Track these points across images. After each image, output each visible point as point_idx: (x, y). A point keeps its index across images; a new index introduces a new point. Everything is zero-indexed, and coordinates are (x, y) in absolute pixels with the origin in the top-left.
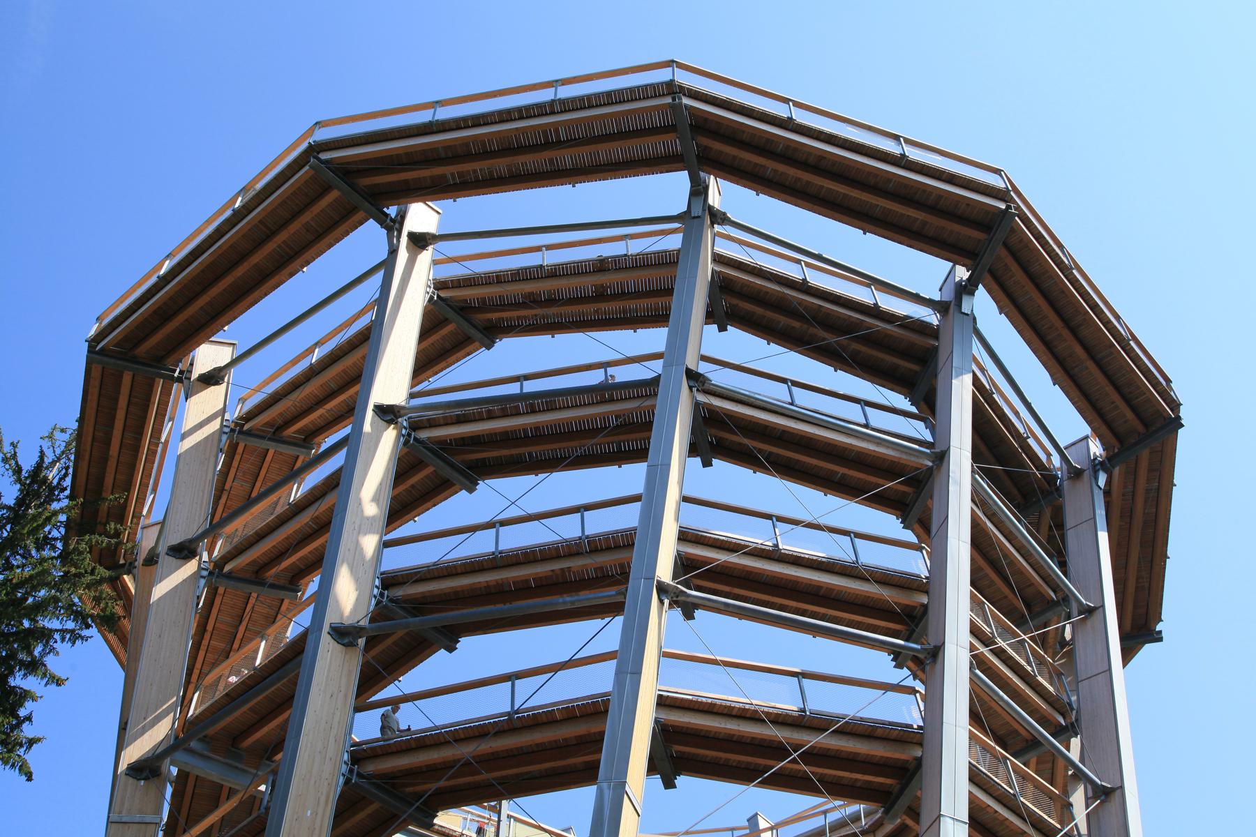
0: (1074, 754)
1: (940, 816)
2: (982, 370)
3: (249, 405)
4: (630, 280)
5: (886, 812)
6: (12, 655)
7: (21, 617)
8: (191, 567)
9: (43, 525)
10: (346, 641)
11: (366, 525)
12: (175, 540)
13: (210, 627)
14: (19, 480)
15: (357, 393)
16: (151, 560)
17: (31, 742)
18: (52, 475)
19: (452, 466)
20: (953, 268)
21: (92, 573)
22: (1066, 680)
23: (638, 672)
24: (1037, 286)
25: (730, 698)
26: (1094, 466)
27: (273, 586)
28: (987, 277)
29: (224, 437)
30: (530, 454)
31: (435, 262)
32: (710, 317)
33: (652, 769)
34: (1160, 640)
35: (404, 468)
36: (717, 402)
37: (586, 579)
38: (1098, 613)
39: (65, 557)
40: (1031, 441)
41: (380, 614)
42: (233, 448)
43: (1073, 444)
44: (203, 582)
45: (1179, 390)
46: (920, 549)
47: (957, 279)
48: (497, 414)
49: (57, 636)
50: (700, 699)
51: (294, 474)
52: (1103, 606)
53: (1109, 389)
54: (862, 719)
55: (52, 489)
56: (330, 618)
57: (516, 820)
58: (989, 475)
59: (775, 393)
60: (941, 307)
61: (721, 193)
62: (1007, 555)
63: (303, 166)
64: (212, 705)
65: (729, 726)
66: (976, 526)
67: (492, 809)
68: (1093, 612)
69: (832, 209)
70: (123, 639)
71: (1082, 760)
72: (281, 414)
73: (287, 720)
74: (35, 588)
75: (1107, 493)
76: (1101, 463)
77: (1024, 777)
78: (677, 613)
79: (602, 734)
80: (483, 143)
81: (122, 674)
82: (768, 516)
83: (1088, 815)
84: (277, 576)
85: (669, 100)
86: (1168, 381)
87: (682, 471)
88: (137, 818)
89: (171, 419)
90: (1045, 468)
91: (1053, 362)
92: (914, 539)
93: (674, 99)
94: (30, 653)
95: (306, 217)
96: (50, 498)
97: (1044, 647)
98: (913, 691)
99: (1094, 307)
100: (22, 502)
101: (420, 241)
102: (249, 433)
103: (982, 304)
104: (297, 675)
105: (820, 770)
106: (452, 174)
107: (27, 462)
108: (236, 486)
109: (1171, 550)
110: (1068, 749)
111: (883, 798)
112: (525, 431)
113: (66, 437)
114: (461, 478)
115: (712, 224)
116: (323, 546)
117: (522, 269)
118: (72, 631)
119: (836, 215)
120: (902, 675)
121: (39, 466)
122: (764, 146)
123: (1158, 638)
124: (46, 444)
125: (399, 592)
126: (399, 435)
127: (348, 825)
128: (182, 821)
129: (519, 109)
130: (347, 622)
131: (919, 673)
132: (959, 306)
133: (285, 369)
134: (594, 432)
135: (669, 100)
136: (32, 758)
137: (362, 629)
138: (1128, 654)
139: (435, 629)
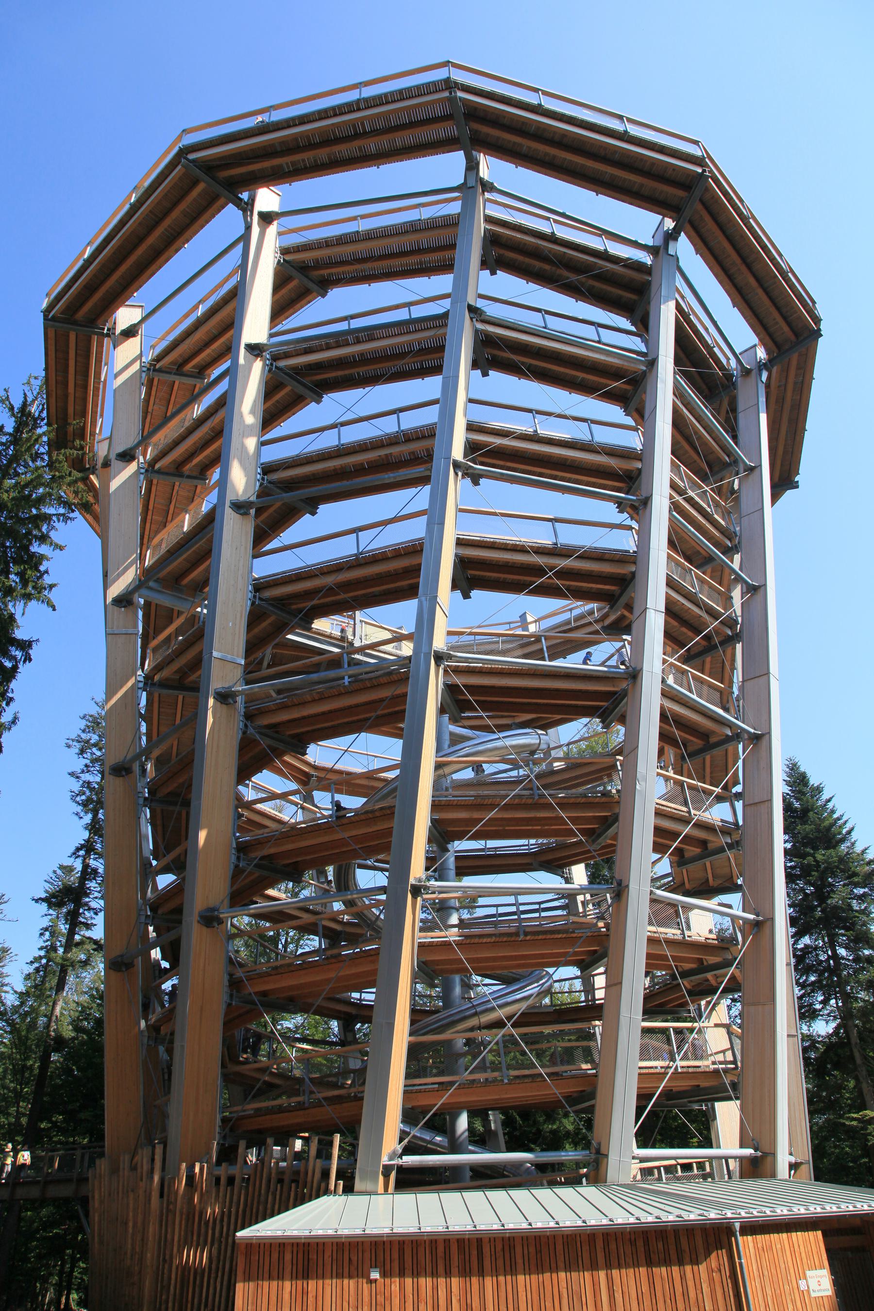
0: (736, 566)
1: (646, 608)
2: (683, 297)
3: (158, 350)
5: (611, 608)
6: (29, 533)
7: (30, 507)
8: (133, 467)
9: (34, 445)
10: (242, 511)
11: (247, 431)
12: (120, 449)
13: (151, 507)
14: (13, 415)
15: (232, 336)
16: (106, 464)
17: (51, 587)
18: (34, 409)
19: (304, 385)
20: (663, 220)
21: (70, 475)
22: (733, 517)
23: (442, 523)
24: (724, 232)
26: (760, 367)
27: (189, 477)
28: (688, 227)
29: (144, 375)
30: (358, 374)
31: (280, 234)
33: (455, 586)
34: (797, 487)
35: (270, 388)
36: (491, 329)
37: (403, 461)
38: (757, 470)
39: (51, 465)
40: (716, 350)
41: (263, 493)
42: (150, 384)
43: (746, 351)
44: (142, 477)
45: (821, 310)
46: (635, 429)
47: (665, 229)
48: (334, 345)
49: (54, 518)
51: (194, 398)
52: (760, 465)
53: (773, 309)
54: (596, 548)
55: (35, 420)
56: (230, 497)
57: (366, 623)
58: (685, 374)
59: (533, 320)
60: (654, 251)
61: (489, 167)
62: (697, 432)
63: (177, 166)
64: (159, 559)
65: (505, 557)
66: (676, 412)
67: (349, 617)
68: (753, 470)
69: (573, 177)
70: (96, 518)
71: (741, 569)
72: (181, 355)
73: (209, 566)
74: (35, 488)
75: (768, 386)
76: (764, 364)
77: (702, 581)
78: (468, 481)
79: (420, 565)
80: (308, 137)
81: (100, 541)
82: (529, 411)
83: (742, 603)
84: (190, 470)
85: (446, 94)
86: (814, 302)
87: (467, 380)
88: (124, 631)
89: (106, 364)
90: (725, 369)
93: (451, 93)
94: (40, 530)
95: (183, 206)
96: (36, 426)
97: (719, 495)
98: (630, 528)
100: (18, 429)
101: (267, 218)
102: (160, 371)
103: (684, 248)
104: (212, 535)
105: (567, 583)
106: (287, 164)
107: (17, 404)
108: (156, 409)
110: (732, 562)
111: (610, 599)
112: (354, 356)
113: (39, 382)
114: (311, 394)
115: (483, 192)
116: (220, 447)
117: (343, 235)
118: (63, 515)
120: (623, 518)
121: (25, 405)
122: (520, 128)
123: (795, 486)
124: (27, 388)
125: (275, 476)
126: (264, 365)
127: (256, 630)
128: (151, 631)
129: (333, 108)
130: (242, 499)
131: (635, 516)
132: (667, 249)
133: (180, 322)
134: (402, 355)
135: (446, 94)
136: (53, 595)
137: (252, 503)
139: (301, 500)
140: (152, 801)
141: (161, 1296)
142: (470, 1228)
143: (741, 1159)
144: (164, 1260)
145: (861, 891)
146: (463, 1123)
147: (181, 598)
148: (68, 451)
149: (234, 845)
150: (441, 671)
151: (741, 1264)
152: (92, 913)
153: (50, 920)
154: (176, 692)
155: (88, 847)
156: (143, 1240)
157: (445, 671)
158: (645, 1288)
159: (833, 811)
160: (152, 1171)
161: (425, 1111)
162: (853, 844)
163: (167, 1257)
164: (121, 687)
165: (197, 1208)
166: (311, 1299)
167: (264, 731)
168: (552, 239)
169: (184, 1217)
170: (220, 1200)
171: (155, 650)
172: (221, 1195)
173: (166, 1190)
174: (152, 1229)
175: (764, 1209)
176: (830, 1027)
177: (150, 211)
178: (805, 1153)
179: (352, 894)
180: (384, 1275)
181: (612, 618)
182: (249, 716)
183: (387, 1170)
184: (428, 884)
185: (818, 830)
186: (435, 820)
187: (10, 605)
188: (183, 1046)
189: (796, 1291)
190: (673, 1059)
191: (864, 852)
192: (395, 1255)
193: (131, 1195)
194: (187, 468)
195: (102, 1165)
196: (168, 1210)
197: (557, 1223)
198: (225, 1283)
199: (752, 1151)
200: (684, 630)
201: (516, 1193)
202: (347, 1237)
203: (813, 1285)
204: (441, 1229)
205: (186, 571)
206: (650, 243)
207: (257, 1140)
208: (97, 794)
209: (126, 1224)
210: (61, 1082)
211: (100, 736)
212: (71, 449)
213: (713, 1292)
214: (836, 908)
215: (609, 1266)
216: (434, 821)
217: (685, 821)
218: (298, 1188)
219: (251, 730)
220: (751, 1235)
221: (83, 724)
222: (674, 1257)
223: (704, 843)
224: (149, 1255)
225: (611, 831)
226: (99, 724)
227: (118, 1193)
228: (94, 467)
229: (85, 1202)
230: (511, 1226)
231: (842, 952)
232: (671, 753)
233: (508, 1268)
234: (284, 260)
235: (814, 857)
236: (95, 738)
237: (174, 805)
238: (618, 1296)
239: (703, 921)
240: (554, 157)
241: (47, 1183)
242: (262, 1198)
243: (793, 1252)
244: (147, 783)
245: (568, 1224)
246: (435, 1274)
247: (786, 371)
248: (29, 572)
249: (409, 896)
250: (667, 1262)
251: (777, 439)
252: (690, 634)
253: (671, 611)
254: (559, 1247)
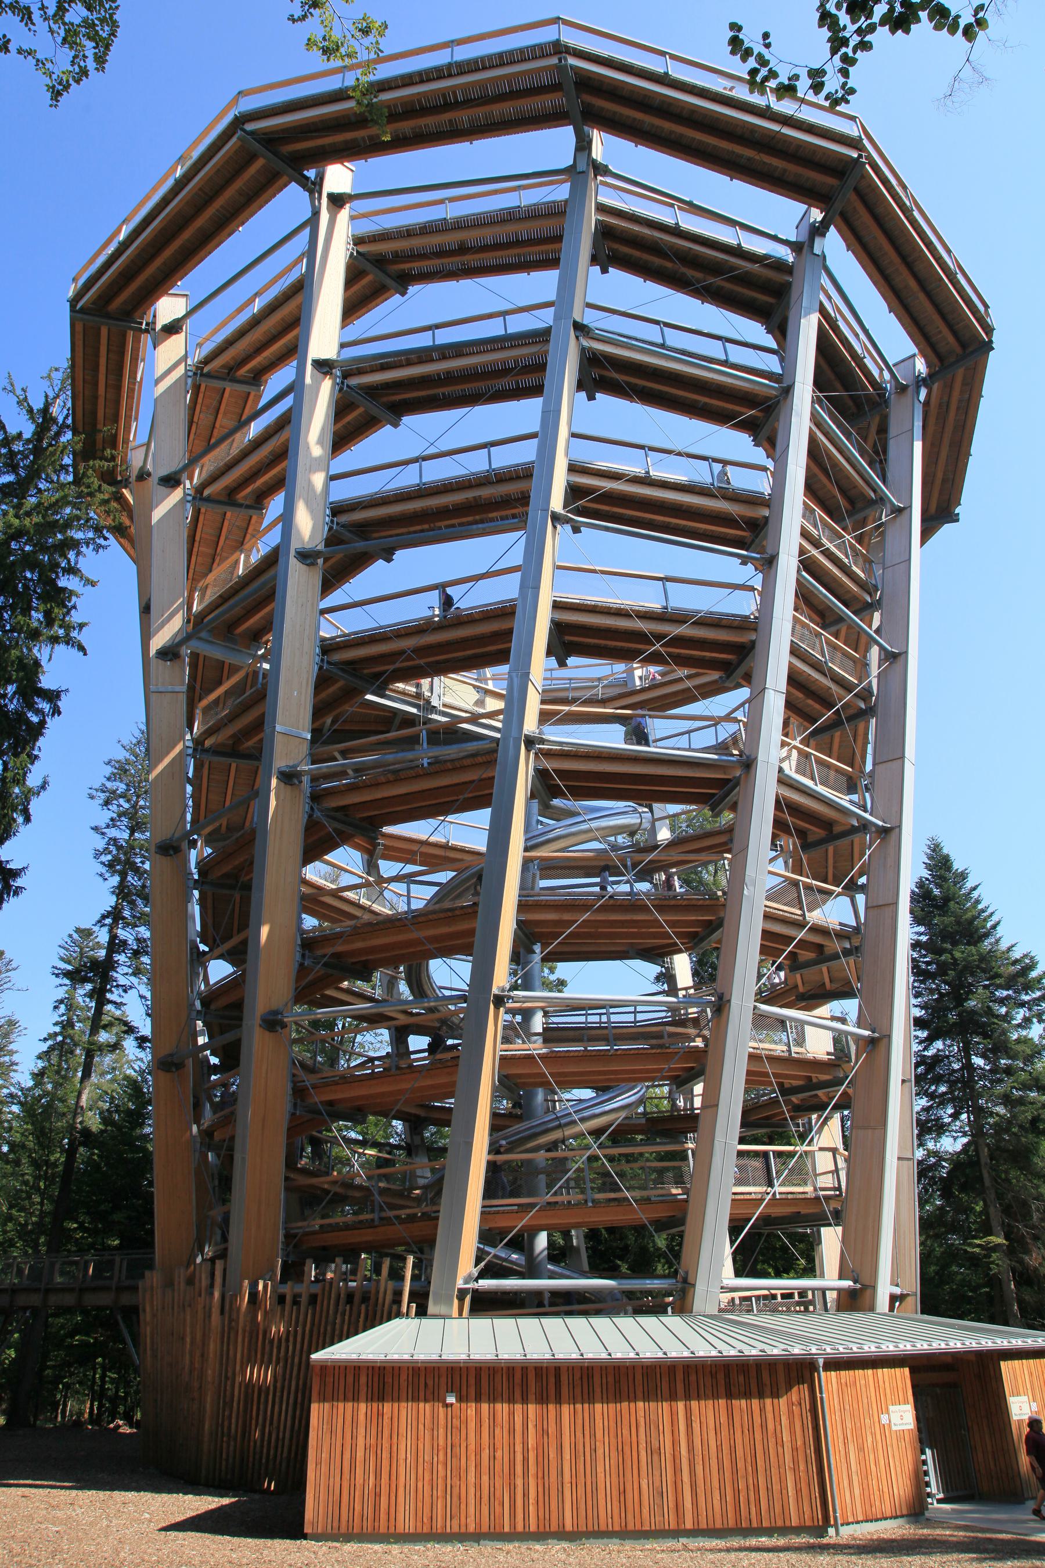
1: (765, 688)
2: (829, 298)
4: (523, 230)
8: (177, 494)
10: (308, 562)
13: (197, 538)
14: (32, 418)
17: (81, 626)
18: (55, 410)
23: (537, 588)
25: (610, 600)
26: (918, 382)
28: (838, 219)
30: (444, 394)
31: (352, 218)
32: (594, 260)
33: (549, 653)
34: (957, 520)
35: (341, 408)
37: (493, 502)
38: (906, 512)
39: (77, 482)
41: (332, 540)
42: (196, 389)
43: (903, 361)
45: (995, 318)
50: (586, 602)
52: (911, 506)
53: (936, 317)
54: (711, 613)
56: (295, 545)
60: (796, 247)
61: (604, 146)
66: (812, 441)
72: (233, 358)
75: (927, 404)
76: (924, 379)
81: (135, 567)
82: (642, 447)
84: (245, 498)
85: (554, 60)
86: (986, 306)
88: (170, 688)
89: (143, 360)
91: (890, 294)
92: (775, 346)
93: (560, 60)
98: (764, 469)
99: (929, 244)
101: (338, 201)
102: (208, 375)
103: (834, 246)
107: (38, 404)
109: (973, 450)
112: (439, 375)
115: (596, 176)
117: (427, 222)
119: (706, 164)
123: (955, 519)
132: (812, 247)
133: (232, 317)
135: (554, 60)
136: (83, 637)
138: (927, 534)
140: (203, 883)
141: (224, 1411)
142: (548, 1356)
143: (840, 1291)
144: (227, 1378)
145: (1005, 993)
146: (542, 1241)
147: (234, 649)
148: (97, 463)
149: (299, 942)
150: (532, 755)
151: (822, 1399)
152: (121, 990)
153: (66, 992)
154: (229, 760)
155: (115, 915)
156: (202, 1355)
157: (536, 754)
158: (724, 1419)
159: (978, 902)
160: (212, 1286)
161: (503, 1233)
162: (997, 941)
163: (230, 1374)
164: (168, 753)
165: (261, 1327)
166: (386, 1421)
167: (332, 814)
168: (676, 231)
169: (247, 1334)
170: (286, 1319)
171: (206, 710)
172: (286, 1313)
173: (227, 1307)
174: (213, 1347)
175: (851, 1345)
176: (958, 1146)
177: (200, 189)
178: (912, 1283)
179: (429, 1002)
180: (460, 1399)
182: (316, 797)
183: (462, 1294)
184: (511, 994)
185: (958, 923)
186: (521, 921)
187: (35, 651)
188: (243, 1159)
189: (877, 1425)
190: (770, 1184)
191: (1009, 949)
192: (472, 1381)
193: (188, 1310)
194: (241, 496)
195: (153, 1278)
196: (230, 1328)
197: (637, 1354)
198: (291, 1401)
199: (851, 1283)
200: (810, 702)
201: (596, 1321)
202: (424, 1362)
203: (895, 1418)
204: (518, 1357)
205: (239, 619)
207: (323, 1257)
208: (125, 854)
209: (183, 1339)
210: (95, 1180)
211: (127, 785)
212: (101, 459)
213: (792, 1423)
214: (973, 1012)
215: (688, 1397)
216: (519, 923)
217: (800, 925)
218: (371, 1312)
219: (317, 814)
220: (835, 1370)
221: (108, 770)
222: (754, 1389)
223: (820, 947)
224: (210, 1372)
225: (715, 936)
226: (126, 771)
227: (173, 1308)
228: (126, 480)
229: (132, 1313)
230: (590, 1356)
231: (978, 1061)
232: (790, 842)
233: (586, 1396)
234: (357, 252)
235: (952, 955)
236: (122, 787)
237: (230, 896)
238: (696, 1426)
239: (818, 1034)
240: (682, 135)
241: (82, 1291)
242: (331, 1318)
243: (877, 1387)
244: (194, 862)
245: (648, 1355)
246: (511, 1400)
247: (949, 387)
248: (56, 610)
249: (492, 1006)
250: (747, 1395)
253: (794, 680)
254: (639, 1377)
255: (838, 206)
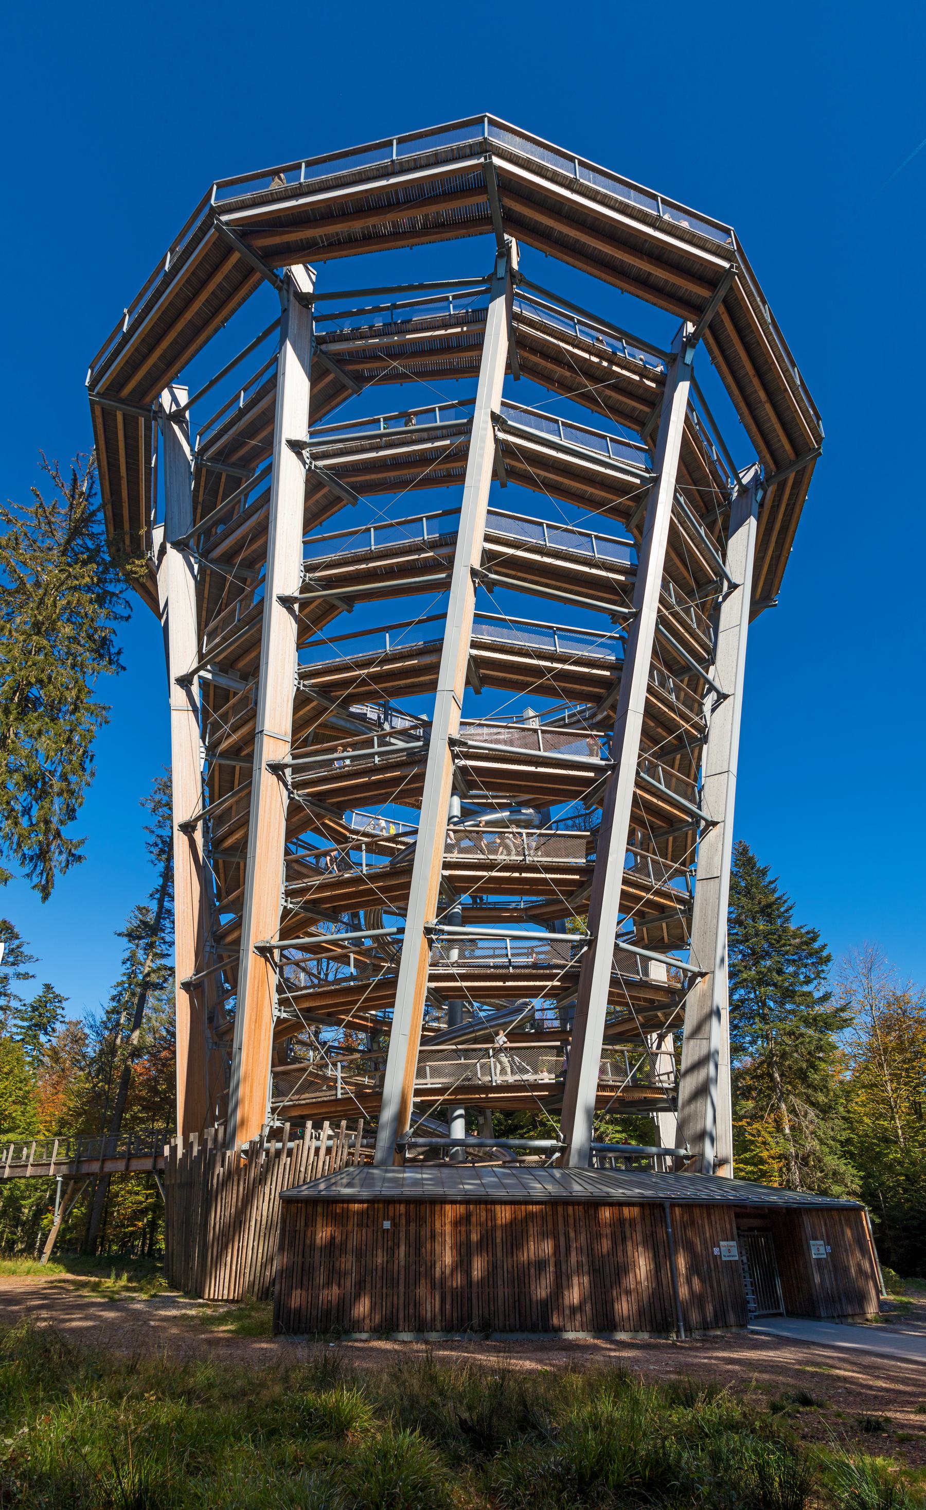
58: (688, 494)
111: (597, 699)
127: (301, 713)
137: (296, 598)
181: (600, 717)
200: (660, 730)
206: (668, 349)
251: (763, 558)
252: (664, 734)
255: (709, 316)
